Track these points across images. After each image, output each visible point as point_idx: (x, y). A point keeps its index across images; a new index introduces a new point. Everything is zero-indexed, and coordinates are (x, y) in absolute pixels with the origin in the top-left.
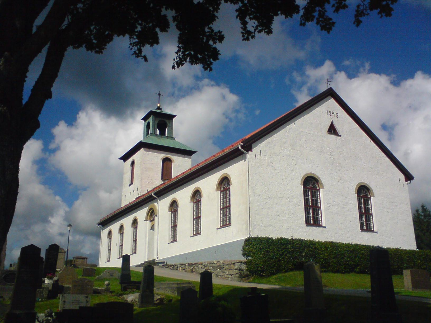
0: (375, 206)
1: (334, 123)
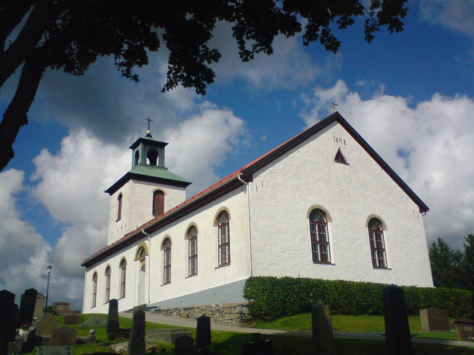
1: (341, 150)
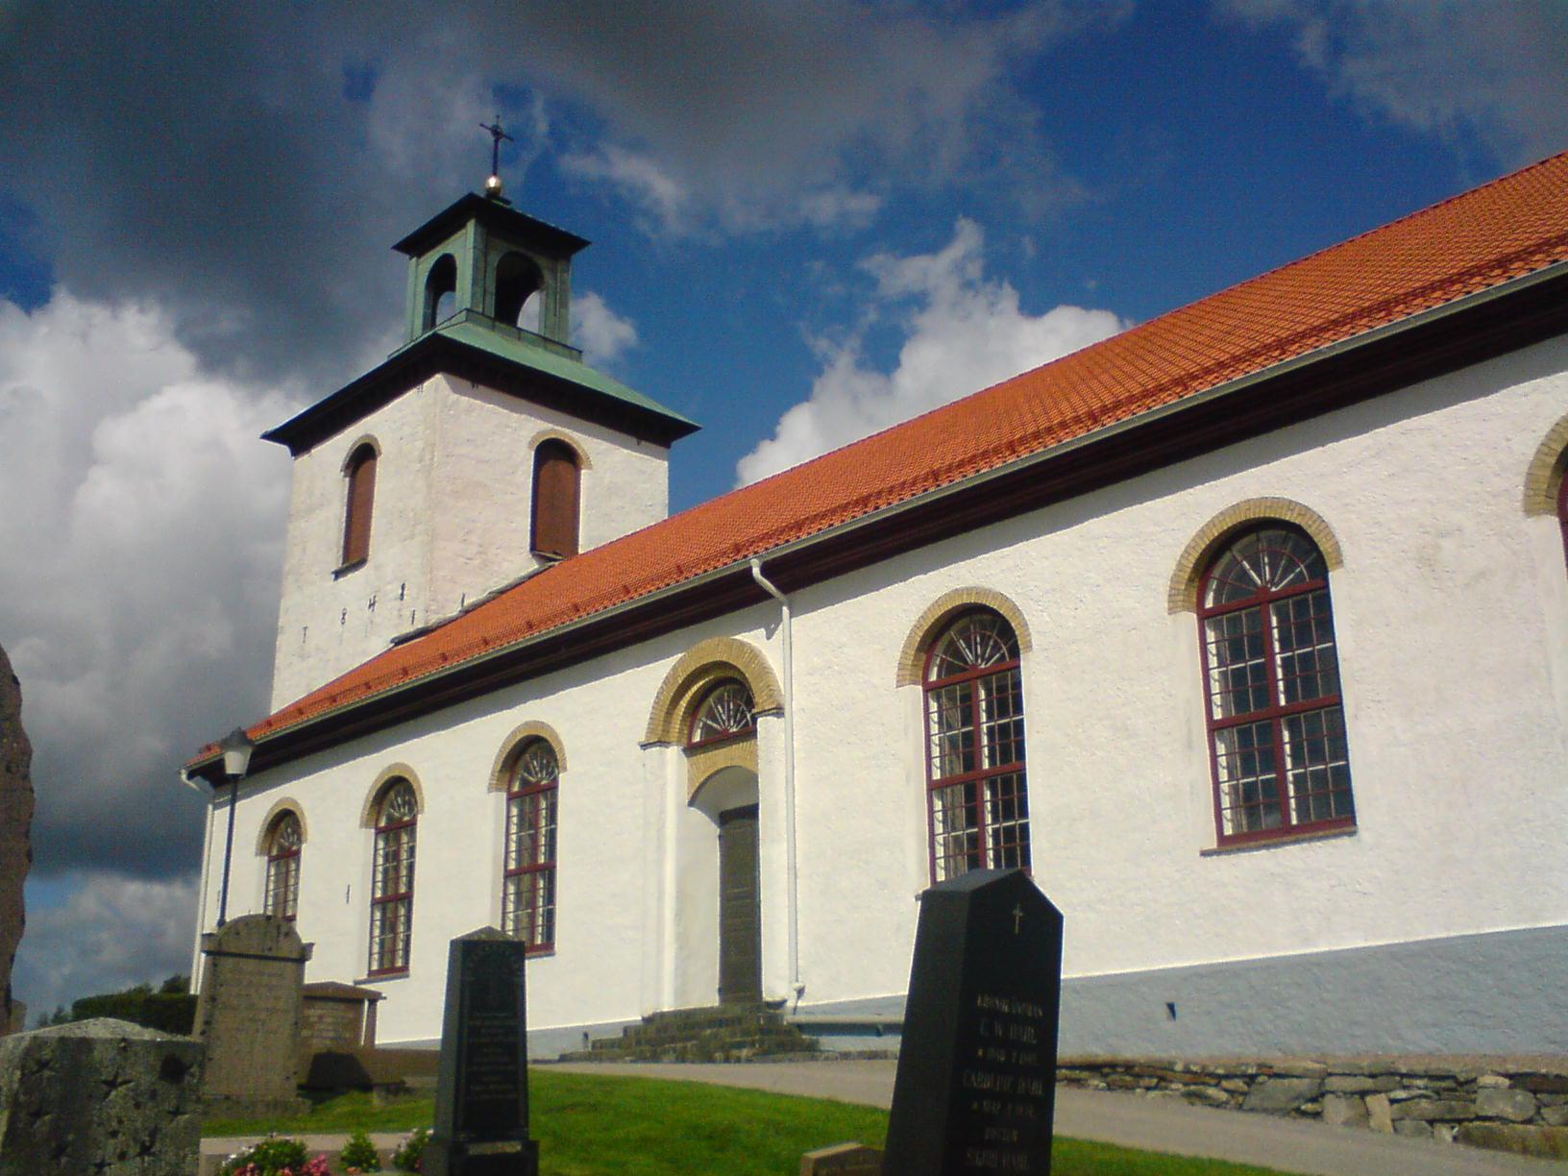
0: (1226, 955)
